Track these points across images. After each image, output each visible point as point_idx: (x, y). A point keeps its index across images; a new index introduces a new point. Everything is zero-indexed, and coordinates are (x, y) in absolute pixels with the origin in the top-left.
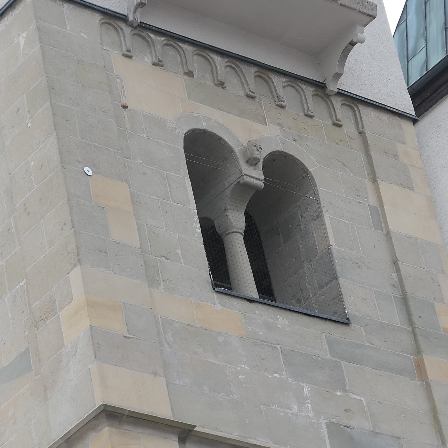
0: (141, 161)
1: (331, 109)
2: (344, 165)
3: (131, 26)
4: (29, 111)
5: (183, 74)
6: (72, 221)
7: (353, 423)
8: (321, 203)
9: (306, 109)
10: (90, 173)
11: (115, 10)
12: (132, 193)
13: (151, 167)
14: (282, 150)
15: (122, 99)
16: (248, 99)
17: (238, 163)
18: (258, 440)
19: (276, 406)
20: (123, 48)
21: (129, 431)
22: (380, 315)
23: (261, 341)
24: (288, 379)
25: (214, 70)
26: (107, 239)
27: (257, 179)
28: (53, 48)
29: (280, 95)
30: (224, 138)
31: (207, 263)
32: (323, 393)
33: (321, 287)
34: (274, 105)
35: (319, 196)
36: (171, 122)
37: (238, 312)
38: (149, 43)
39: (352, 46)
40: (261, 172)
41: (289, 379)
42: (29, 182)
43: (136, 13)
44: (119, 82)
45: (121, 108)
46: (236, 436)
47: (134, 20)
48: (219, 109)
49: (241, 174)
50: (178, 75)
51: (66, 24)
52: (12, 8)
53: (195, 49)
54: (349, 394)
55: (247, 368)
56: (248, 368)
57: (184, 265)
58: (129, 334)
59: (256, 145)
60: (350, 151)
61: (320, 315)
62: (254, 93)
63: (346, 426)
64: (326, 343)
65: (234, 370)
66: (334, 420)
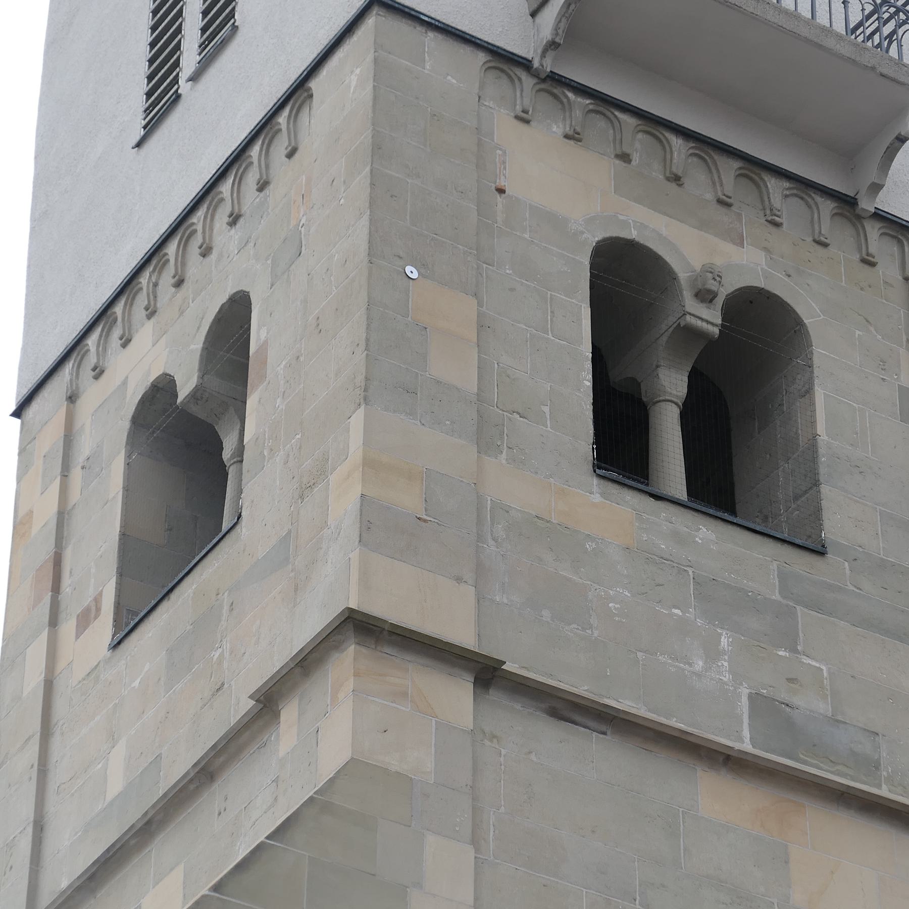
0: (511, 272)
1: (861, 238)
2: (867, 321)
3: (537, 77)
4: (344, 182)
5: (613, 157)
6: (367, 340)
7: (796, 701)
8: (815, 371)
9: (817, 232)
10: (415, 275)
11: (511, 50)
12: (480, 315)
13: (526, 282)
14: (763, 287)
15: (500, 179)
16: (719, 207)
17: (682, 296)
18: (621, 702)
19: (666, 656)
20: (518, 107)
21: (392, 655)
22: (883, 548)
23: (662, 558)
24: (696, 620)
25: (668, 157)
26: (421, 373)
27: (708, 322)
28: (394, 91)
29: (774, 206)
30: (664, 257)
31: (592, 431)
32: (754, 649)
33: (796, 498)
34: (763, 221)
35: (813, 362)
36: (577, 222)
37: (630, 510)
38: (564, 104)
39: (901, 144)
40: (719, 313)
41: (698, 620)
42: (327, 285)
43: (545, 57)
44: (499, 155)
45: (495, 192)
46: (584, 690)
47: (541, 67)
48: (665, 214)
49: (683, 313)
50: (605, 157)
51: (425, 61)
52: (351, 33)
53: (640, 122)
54: (800, 657)
55: (627, 593)
56: (629, 595)
57: (551, 430)
58: (426, 515)
59: (713, 271)
60: (884, 303)
61: (773, 533)
62: (730, 198)
63: (784, 704)
64: (776, 576)
65: (603, 593)
66: (765, 691)
